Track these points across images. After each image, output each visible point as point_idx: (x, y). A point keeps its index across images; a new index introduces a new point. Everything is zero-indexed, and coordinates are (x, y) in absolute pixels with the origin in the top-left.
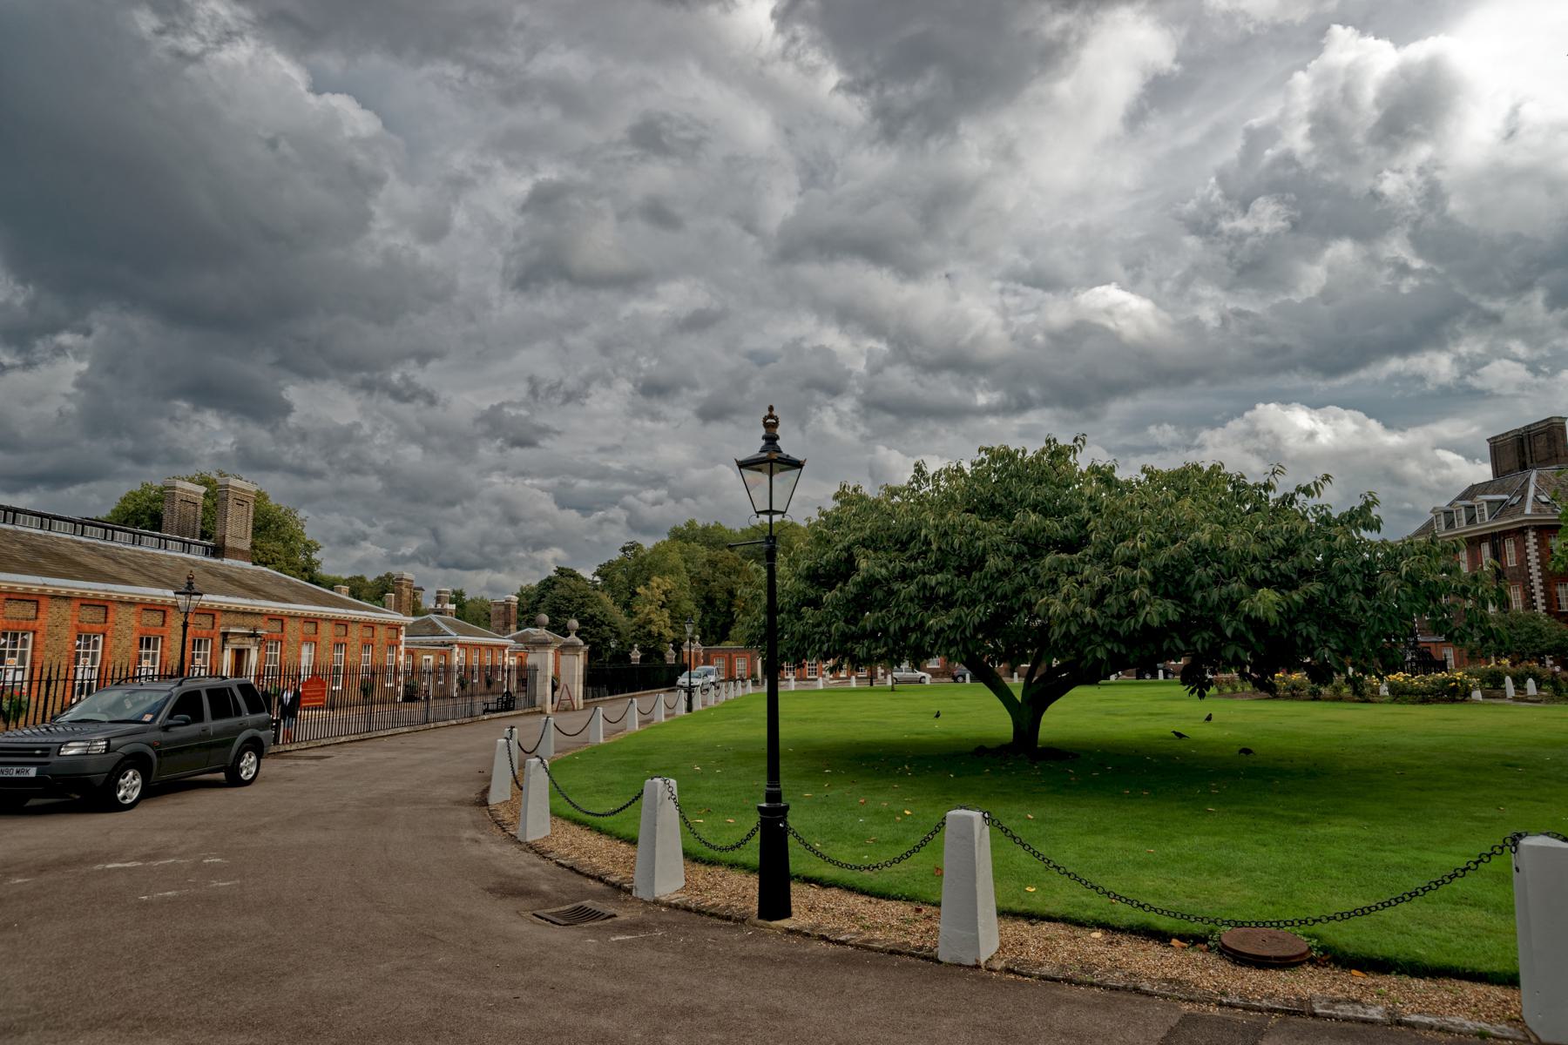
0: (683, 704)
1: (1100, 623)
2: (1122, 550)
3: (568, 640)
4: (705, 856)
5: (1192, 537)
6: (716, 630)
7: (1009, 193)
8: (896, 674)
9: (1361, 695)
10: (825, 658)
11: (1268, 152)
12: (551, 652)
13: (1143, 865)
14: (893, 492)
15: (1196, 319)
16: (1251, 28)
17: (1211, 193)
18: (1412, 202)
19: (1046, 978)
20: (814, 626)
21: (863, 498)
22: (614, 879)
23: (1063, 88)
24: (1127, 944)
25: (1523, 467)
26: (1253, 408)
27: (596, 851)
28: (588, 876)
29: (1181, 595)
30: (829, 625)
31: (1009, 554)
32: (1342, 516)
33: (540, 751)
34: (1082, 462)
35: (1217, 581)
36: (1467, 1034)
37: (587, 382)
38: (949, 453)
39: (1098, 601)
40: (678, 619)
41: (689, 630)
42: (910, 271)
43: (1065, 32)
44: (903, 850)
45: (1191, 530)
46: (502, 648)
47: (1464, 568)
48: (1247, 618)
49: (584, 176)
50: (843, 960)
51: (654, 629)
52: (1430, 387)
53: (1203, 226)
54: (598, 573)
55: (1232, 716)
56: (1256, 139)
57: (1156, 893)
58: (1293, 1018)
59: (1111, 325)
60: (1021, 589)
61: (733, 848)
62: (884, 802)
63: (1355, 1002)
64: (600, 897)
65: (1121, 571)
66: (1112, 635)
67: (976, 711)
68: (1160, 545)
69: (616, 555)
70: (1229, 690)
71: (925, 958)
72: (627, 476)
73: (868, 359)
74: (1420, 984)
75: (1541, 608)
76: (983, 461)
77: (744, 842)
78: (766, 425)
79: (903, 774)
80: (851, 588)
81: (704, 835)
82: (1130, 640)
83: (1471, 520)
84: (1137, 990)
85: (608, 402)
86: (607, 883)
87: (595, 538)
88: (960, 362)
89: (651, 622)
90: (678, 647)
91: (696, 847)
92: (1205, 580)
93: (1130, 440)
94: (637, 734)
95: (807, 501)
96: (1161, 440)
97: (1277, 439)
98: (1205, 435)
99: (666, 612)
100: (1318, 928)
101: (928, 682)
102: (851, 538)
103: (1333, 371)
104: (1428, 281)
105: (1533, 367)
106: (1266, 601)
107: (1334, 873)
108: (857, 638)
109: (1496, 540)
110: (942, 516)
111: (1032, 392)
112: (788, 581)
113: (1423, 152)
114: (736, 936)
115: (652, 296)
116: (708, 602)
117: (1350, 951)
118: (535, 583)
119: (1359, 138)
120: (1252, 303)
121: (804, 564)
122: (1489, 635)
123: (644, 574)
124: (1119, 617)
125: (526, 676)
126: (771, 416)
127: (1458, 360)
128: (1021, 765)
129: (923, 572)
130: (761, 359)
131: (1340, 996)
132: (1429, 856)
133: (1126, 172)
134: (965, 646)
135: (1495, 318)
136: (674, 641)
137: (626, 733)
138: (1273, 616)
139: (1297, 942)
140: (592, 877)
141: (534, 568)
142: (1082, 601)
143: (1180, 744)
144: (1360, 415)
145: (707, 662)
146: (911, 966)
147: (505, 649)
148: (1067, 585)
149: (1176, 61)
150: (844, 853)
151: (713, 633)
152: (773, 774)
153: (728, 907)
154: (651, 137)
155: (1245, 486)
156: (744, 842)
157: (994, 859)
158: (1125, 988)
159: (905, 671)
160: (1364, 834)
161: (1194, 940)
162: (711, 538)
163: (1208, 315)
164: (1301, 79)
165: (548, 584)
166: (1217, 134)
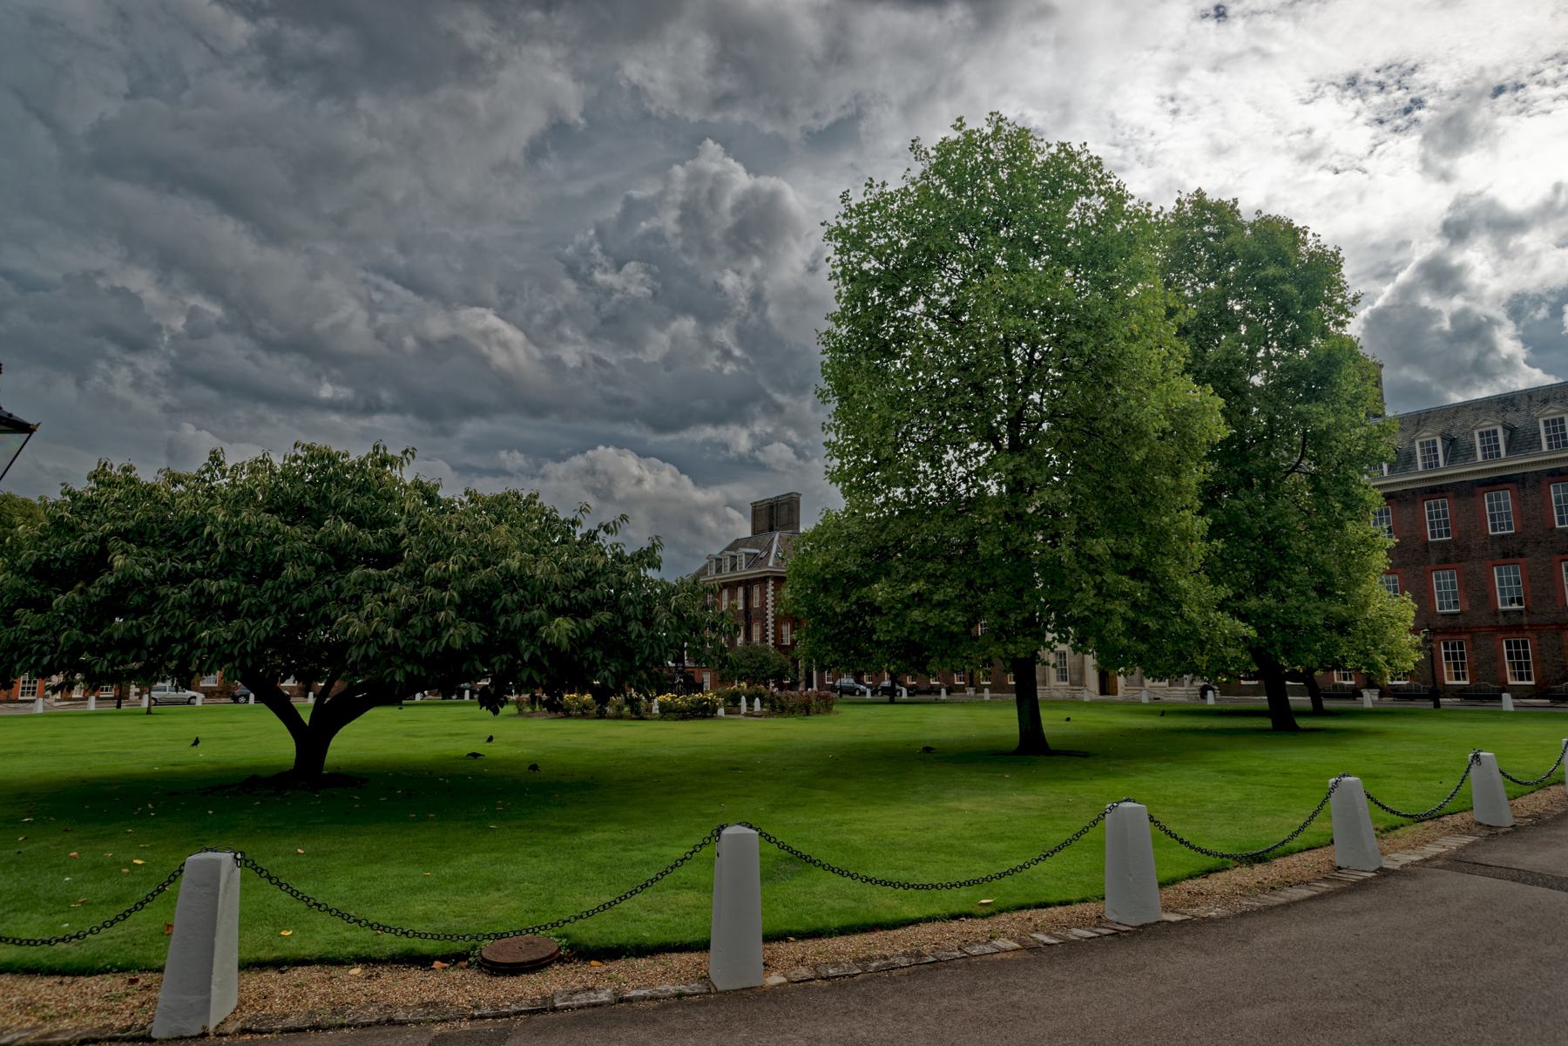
1: (401, 644)
2: (432, 570)
5: (503, 563)
8: (154, 694)
9: (638, 713)
10: (46, 673)
11: (643, 224)
13: (414, 891)
14: (176, 480)
16: (653, 109)
17: (591, 244)
19: (288, 1030)
20: (32, 633)
24: (386, 975)
25: (771, 529)
26: (594, 448)
30: (57, 634)
31: (311, 562)
32: (633, 554)
35: (521, 607)
38: (260, 446)
39: (401, 621)
42: (273, 235)
45: (504, 556)
48: (544, 642)
52: (732, 454)
55: (518, 734)
57: (426, 918)
58: (536, 1017)
59: (485, 349)
60: (319, 603)
63: (589, 989)
65: (430, 592)
66: (412, 657)
67: (254, 736)
68: (472, 569)
70: (528, 710)
71: (134, 1039)
73: (189, 318)
74: (641, 963)
75: (771, 642)
76: (296, 458)
80: (95, 591)
83: (733, 568)
84: (391, 1022)
88: (313, 349)
92: (509, 604)
96: (509, 466)
98: (550, 466)
100: (568, 928)
101: (199, 702)
102: (108, 526)
103: (662, 427)
105: (799, 454)
106: (561, 628)
109: (748, 584)
110: (237, 513)
111: (385, 395)
117: (591, 944)
119: (716, 235)
121: (27, 556)
124: (423, 638)
127: (752, 436)
128: (306, 794)
129: (202, 576)
131: (579, 987)
134: (243, 663)
135: (779, 408)
139: (550, 942)
142: (385, 621)
144: (675, 469)
148: (371, 603)
150: (31, 925)
155: (556, 521)
158: (378, 1023)
159: (165, 689)
161: (453, 959)
163: (570, 356)
166: (600, 195)
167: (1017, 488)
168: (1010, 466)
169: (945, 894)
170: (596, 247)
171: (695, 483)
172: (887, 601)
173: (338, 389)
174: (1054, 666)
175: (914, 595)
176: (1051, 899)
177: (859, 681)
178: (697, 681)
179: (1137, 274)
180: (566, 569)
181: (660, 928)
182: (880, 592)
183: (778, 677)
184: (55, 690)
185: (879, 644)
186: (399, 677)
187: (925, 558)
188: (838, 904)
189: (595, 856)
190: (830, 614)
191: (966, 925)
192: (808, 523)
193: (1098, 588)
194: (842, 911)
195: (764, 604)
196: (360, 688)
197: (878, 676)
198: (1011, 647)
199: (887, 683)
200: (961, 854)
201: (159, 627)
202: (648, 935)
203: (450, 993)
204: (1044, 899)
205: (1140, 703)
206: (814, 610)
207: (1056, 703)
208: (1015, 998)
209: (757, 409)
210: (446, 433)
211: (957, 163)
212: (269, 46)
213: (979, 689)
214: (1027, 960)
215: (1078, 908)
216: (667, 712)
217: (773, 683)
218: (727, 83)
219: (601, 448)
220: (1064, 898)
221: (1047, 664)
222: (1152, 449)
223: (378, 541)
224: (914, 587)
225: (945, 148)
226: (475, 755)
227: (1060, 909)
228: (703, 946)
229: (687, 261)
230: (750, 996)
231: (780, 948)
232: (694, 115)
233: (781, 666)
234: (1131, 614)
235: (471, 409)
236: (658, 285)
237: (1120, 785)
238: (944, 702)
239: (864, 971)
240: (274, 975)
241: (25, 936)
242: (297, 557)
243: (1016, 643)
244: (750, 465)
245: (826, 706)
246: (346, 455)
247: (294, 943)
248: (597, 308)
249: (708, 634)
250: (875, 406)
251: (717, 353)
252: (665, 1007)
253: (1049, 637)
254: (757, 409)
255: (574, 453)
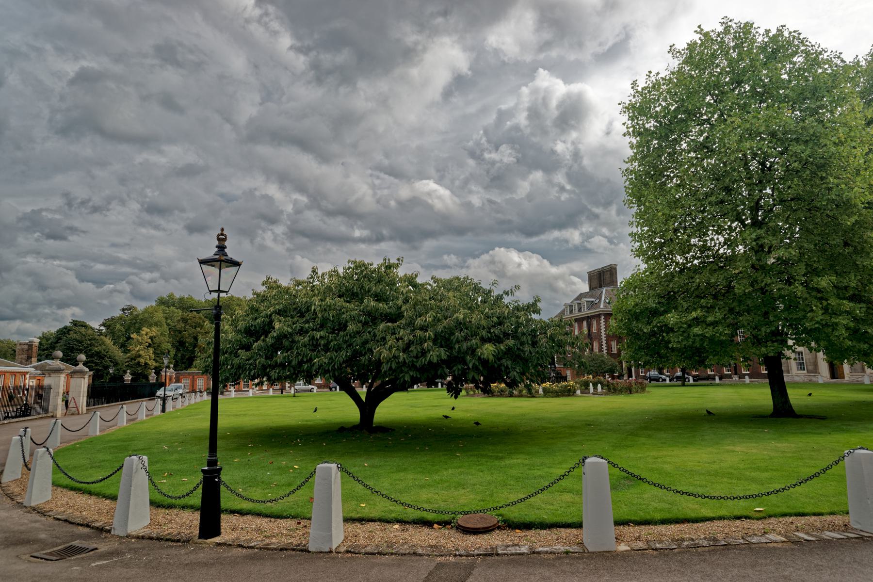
0: (160, 408)
2: (419, 322)
3: (77, 368)
4: (165, 503)
6: (184, 361)
7: (381, 122)
9: (531, 394)
11: (508, 123)
12: (63, 377)
13: (422, 487)
14: (299, 283)
15: (470, 202)
16: (506, 59)
17: (481, 139)
18: (568, 157)
21: (279, 286)
22: (97, 524)
23: (414, 72)
24: (412, 530)
25: (601, 286)
26: (493, 249)
27: (86, 507)
28: (78, 524)
29: (449, 346)
30: (255, 360)
33: (48, 444)
34: (401, 272)
35: (466, 339)
36: (560, 553)
37: (109, 200)
38: (333, 263)
39: (406, 349)
40: (159, 354)
41: (166, 361)
42: (324, 158)
43: (416, 43)
44: (291, 489)
46: (25, 374)
47: (576, 333)
48: (480, 358)
49: (118, 69)
50: (252, 558)
51: (142, 361)
52: (570, 245)
53: (475, 154)
54: (103, 325)
55: (471, 406)
56: (503, 116)
57: (428, 501)
59: (430, 201)
60: (366, 342)
61: (184, 496)
62: (284, 462)
64: (87, 537)
65: (419, 333)
66: (413, 367)
67: (340, 407)
68: (439, 320)
69: (118, 313)
70: (472, 393)
71: (301, 550)
72: (128, 263)
73: (294, 205)
74: (544, 532)
75: (605, 351)
76: (349, 268)
77: (191, 492)
78: (219, 239)
79: (296, 445)
81: (165, 490)
82: (422, 369)
83: (580, 310)
84: (415, 553)
85: (122, 215)
86: (93, 528)
87: (105, 302)
88: (348, 213)
89: (140, 356)
90: (158, 372)
91: (159, 497)
93: (431, 261)
94: (125, 428)
95: (244, 286)
96: (449, 263)
97: (504, 266)
98: (471, 261)
99: (151, 350)
100: (502, 511)
101: (315, 391)
102: (272, 309)
103: (530, 234)
104: (572, 196)
105: (611, 241)
106: (488, 350)
107: (512, 482)
108: (273, 367)
109: (589, 319)
111: (385, 232)
112: (229, 333)
113: (574, 135)
114: (183, 551)
115: (160, 152)
116: (180, 344)
118: (54, 330)
119: (549, 123)
120: (497, 197)
121: (241, 325)
122: (582, 364)
123: (137, 325)
124: (417, 357)
125: (42, 393)
126: (222, 234)
127: (582, 234)
128: (365, 435)
129: (313, 330)
130: (228, 198)
131: (510, 543)
132: (553, 470)
133: (441, 121)
134: (334, 374)
135: (597, 216)
136: (156, 368)
137: (117, 428)
138: (491, 358)
139: (493, 518)
140: (82, 525)
141: (56, 320)
143: (446, 421)
144: (540, 257)
145: (178, 381)
146: (292, 556)
147: (27, 375)
149: (470, 69)
150: (256, 493)
151: (183, 363)
152: (213, 449)
153: (179, 533)
154: (167, 54)
156: (191, 492)
157: (342, 489)
158: (409, 553)
159: (300, 385)
160: (526, 462)
161: (445, 524)
162: (185, 305)
163: (476, 200)
164: (525, 90)
165: (65, 331)
166: (484, 110)
167: (760, 249)
168: (754, 236)
169: (730, 503)
170: (484, 140)
171: (551, 263)
172: (677, 323)
173: (362, 231)
174: (795, 359)
175: (694, 319)
176: (807, 511)
177: (661, 373)
178: (564, 375)
179: (842, 100)
180: (487, 317)
181: (553, 514)
182: (672, 318)
183: (611, 372)
184: (256, 385)
185: (673, 350)
186: (407, 378)
187: (699, 297)
188: (660, 506)
189: (514, 472)
190: (641, 333)
191: (746, 523)
192: (622, 277)
193: (826, 310)
194: (661, 510)
195: (599, 329)
196: (388, 383)
197: (673, 369)
198: (763, 349)
199: (679, 374)
200: (739, 479)
201: (297, 356)
202: (547, 517)
203: (443, 542)
204: (801, 510)
205: (863, 384)
206: (631, 332)
207: (797, 385)
208: (786, 573)
209: (583, 219)
210: (415, 248)
211: (700, 55)
212: (315, 66)
213: (742, 376)
214: (793, 549)
215: (829, 518)
216: (547, 393)
217: (608, 375)
218: (547, 35)
219: (497, 249)
220: (816, 510)
221: (789, 358)
222: (860, 215)
223: (390, 307)
224: (694, 314)
225: (692, 46)
226: (446, 417)
227: (814, 518)
228: (579, 526)
229: (535, 140)
230: (607, 556)
231: (625, 529)
232: (528, 58)
233: (612, 365)
234: (852, 325)
235: (428, 234)
236: (520, 155)
237: (854, 438)
238: (718, 385)
239: (679, 547)
240: (359, 525)
241: (255, 498)
242: (353, 319)
243: (766, 347)
244: (582, 251)
245: (642, 389)
246: (372, 264)
247: (367, 510)
248: (488, 172)
249: (568, 348)
250: (660, 208)
251: (557, 189)
252: (559, 558)
253: (790, 342)
254: (583, 219)
255: (482, 253)
